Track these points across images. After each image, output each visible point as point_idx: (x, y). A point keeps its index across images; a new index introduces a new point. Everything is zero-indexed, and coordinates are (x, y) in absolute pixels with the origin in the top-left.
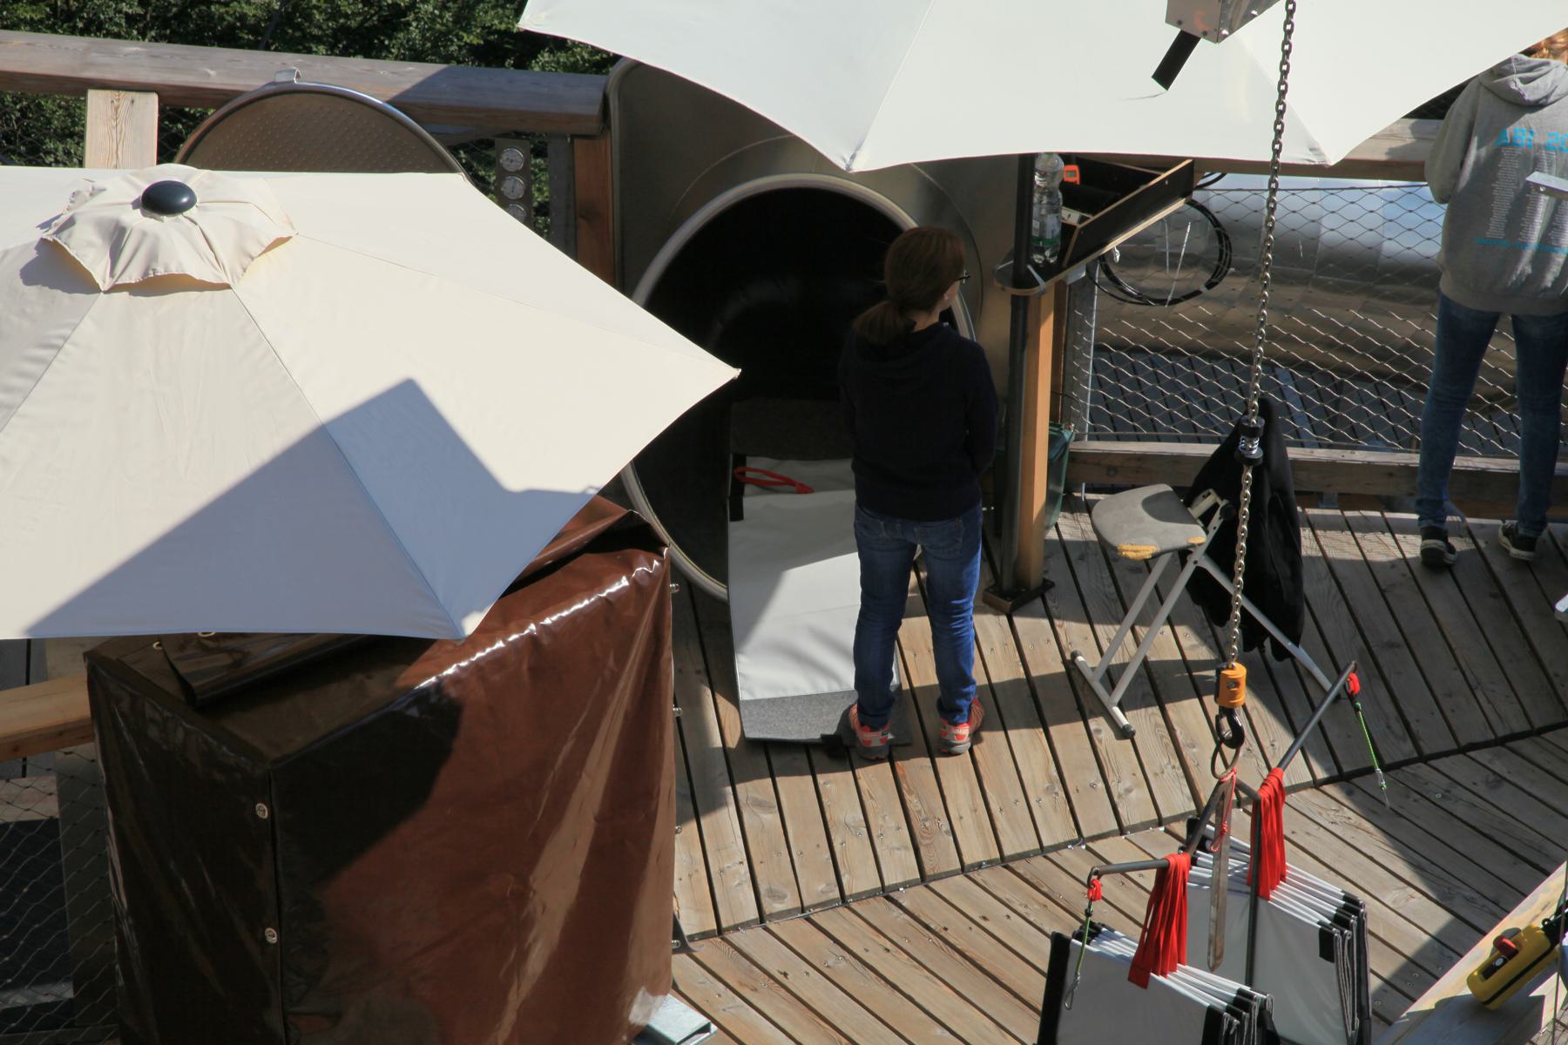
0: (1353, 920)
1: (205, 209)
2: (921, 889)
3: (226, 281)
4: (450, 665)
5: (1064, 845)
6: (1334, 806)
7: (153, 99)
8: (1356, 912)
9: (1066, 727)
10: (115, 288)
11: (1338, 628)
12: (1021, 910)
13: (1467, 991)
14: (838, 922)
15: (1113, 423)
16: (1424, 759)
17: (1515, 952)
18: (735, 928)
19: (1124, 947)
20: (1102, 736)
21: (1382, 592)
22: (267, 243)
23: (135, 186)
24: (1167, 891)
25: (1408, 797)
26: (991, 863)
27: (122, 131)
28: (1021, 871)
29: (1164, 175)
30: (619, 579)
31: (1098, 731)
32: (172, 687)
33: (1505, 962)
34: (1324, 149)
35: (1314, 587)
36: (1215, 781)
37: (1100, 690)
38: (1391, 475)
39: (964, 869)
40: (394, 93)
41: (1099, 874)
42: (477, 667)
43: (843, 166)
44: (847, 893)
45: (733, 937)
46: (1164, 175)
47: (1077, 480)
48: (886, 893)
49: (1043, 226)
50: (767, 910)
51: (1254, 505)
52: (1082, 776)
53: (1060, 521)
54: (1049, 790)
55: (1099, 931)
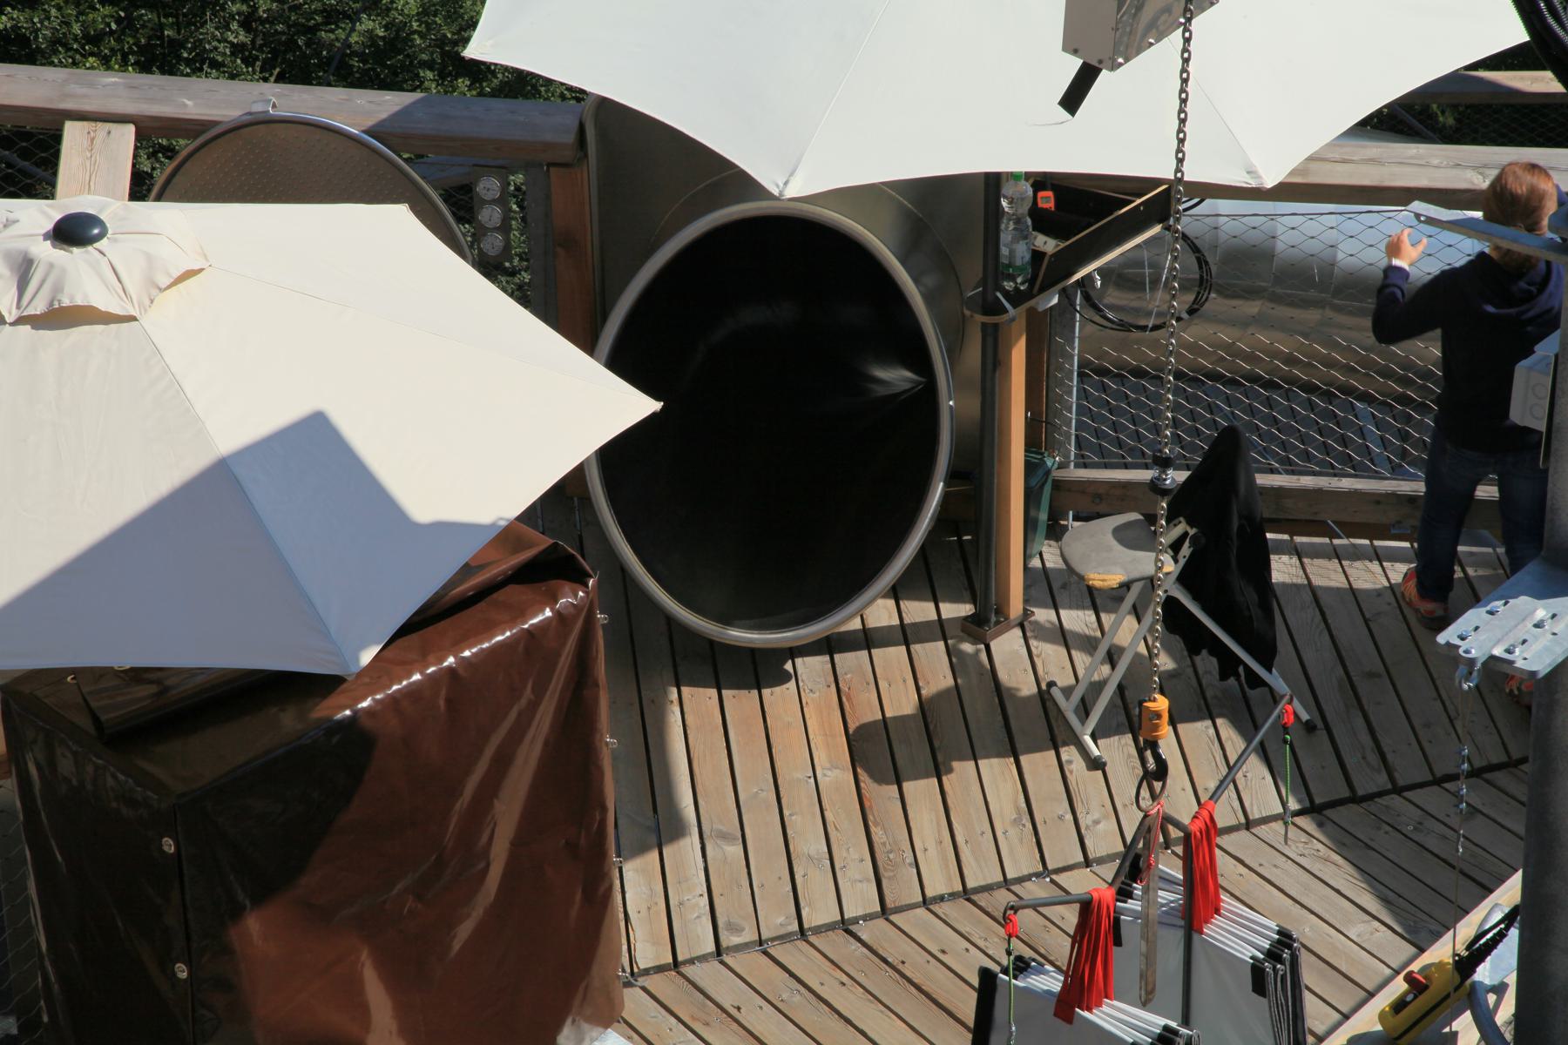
0: (1286, 955)
1: (116, 240)
2: (881, 922)
3: (133, 313)
4: (364, 699)
5: (1028, 878)
6: (1304, 838)
7: (130, 130)
8: (1290, 947)
9: (1037, 756)
10: (20, 321)
11: (1318, 654)
12: (981, 943)
13: (1379, 1028)
14: (795, 956)
15: (1102, 452)
16: (1398, 790)
17: (1426, 987)
18: (691, 961)
19: (1051, 982)
20: (1073, 767)
21: (1366, 621)
22: (176, 274)
23: (49, 217)
24: (1096, 930)
25: (1379, 828)
26: (953, 896)
27: (94, 165)
28: (982, 904)
29: (1139, 201)
30: (543, 611)
31: (1070, 762)
32: (84, 722)
33: (1416, 997)
34: (1261, 172)
35: (1299, 617)
36: (1141, 815)
37: (1073, 720)
38: (1378, 503)
39: (926, 902)
40: (370, 122)
41: (1015, 909)
42: (394, 700)
43: (776, 192)
44: (806, 926)
45: (688, 970)
46: (1139, 201)
47: (1056, 507)
48: (845, 926)
49: (1012, 252)
50: (724, 943)
51: (1223, 534)
52: (1050, 807)
53: (1045, 549)
54: (1017, 822)
55: (1028, 965)
